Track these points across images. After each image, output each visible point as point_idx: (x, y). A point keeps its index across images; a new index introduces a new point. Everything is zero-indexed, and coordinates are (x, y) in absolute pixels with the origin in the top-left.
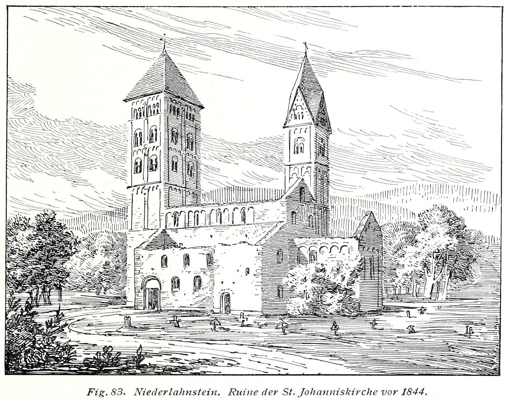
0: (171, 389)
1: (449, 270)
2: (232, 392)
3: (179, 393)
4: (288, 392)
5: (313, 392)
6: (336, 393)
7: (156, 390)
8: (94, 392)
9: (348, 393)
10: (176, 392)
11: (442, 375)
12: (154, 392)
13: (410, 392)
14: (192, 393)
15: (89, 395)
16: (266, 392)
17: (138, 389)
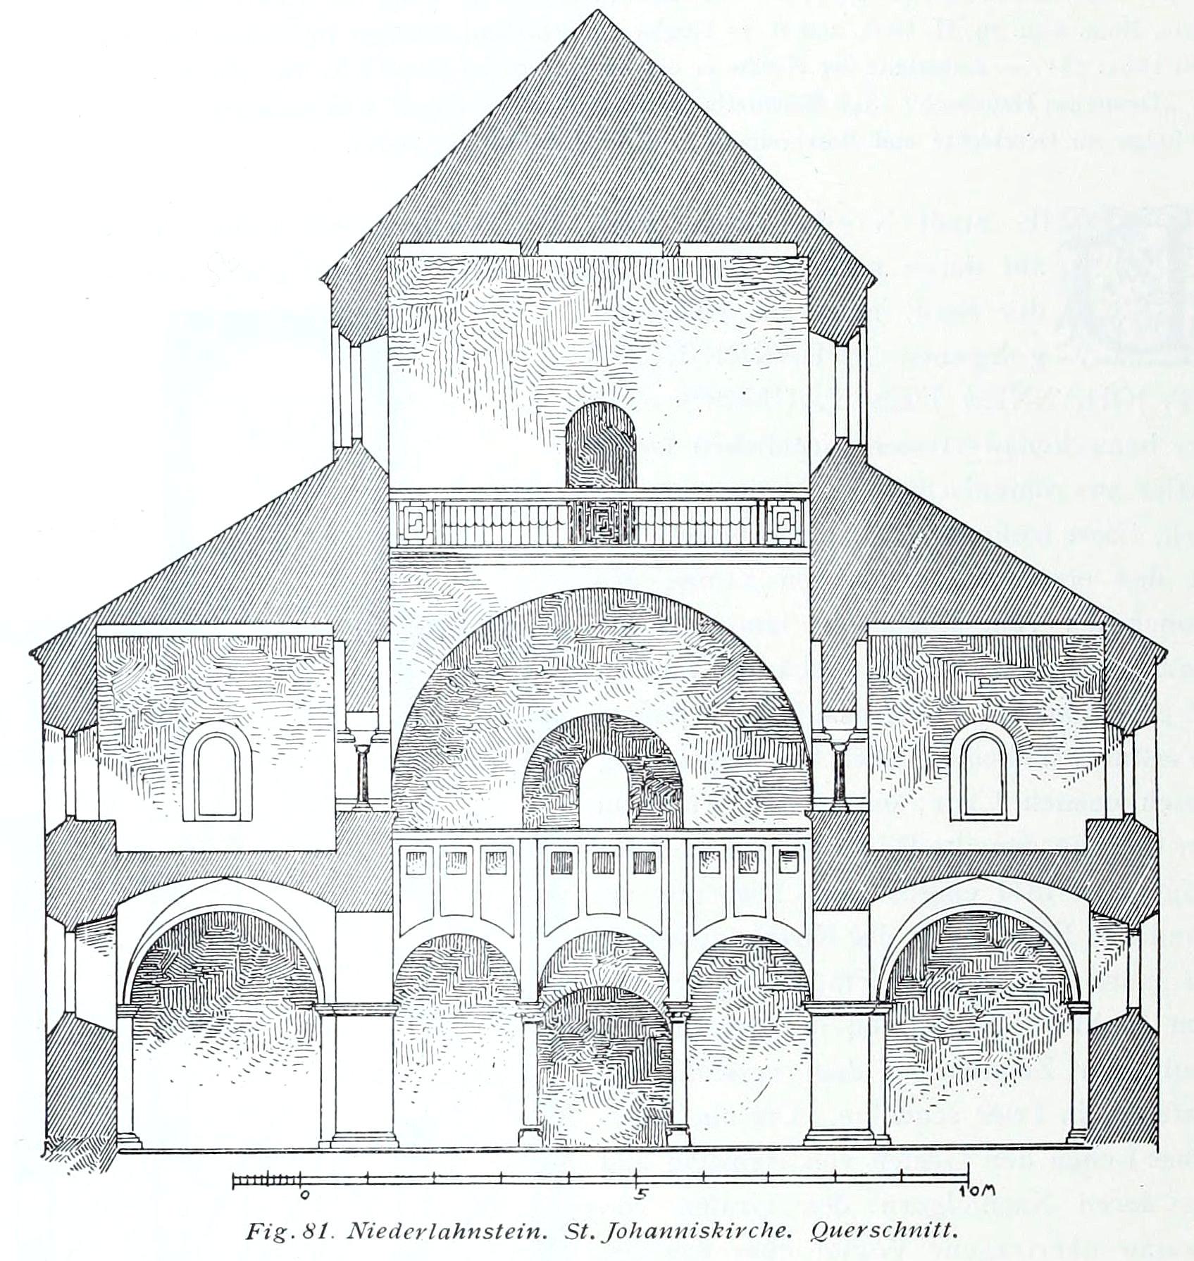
0: (435, 1225)
2: (614, 1231)
3: (451, 1234)
4: (578, 1231)
5: (635, 1231)
6: (689, 1233)
7: (398, 1226)
8: (262, 1233)
9: (718, 1234)
10: (651, 1231)
11: (880, 1175)
12: (395, 1231)
13: (311, 1231)
14: (482, 1233)
15: (250, 1237)
16: (399, 1230)
17: (356, 1224)
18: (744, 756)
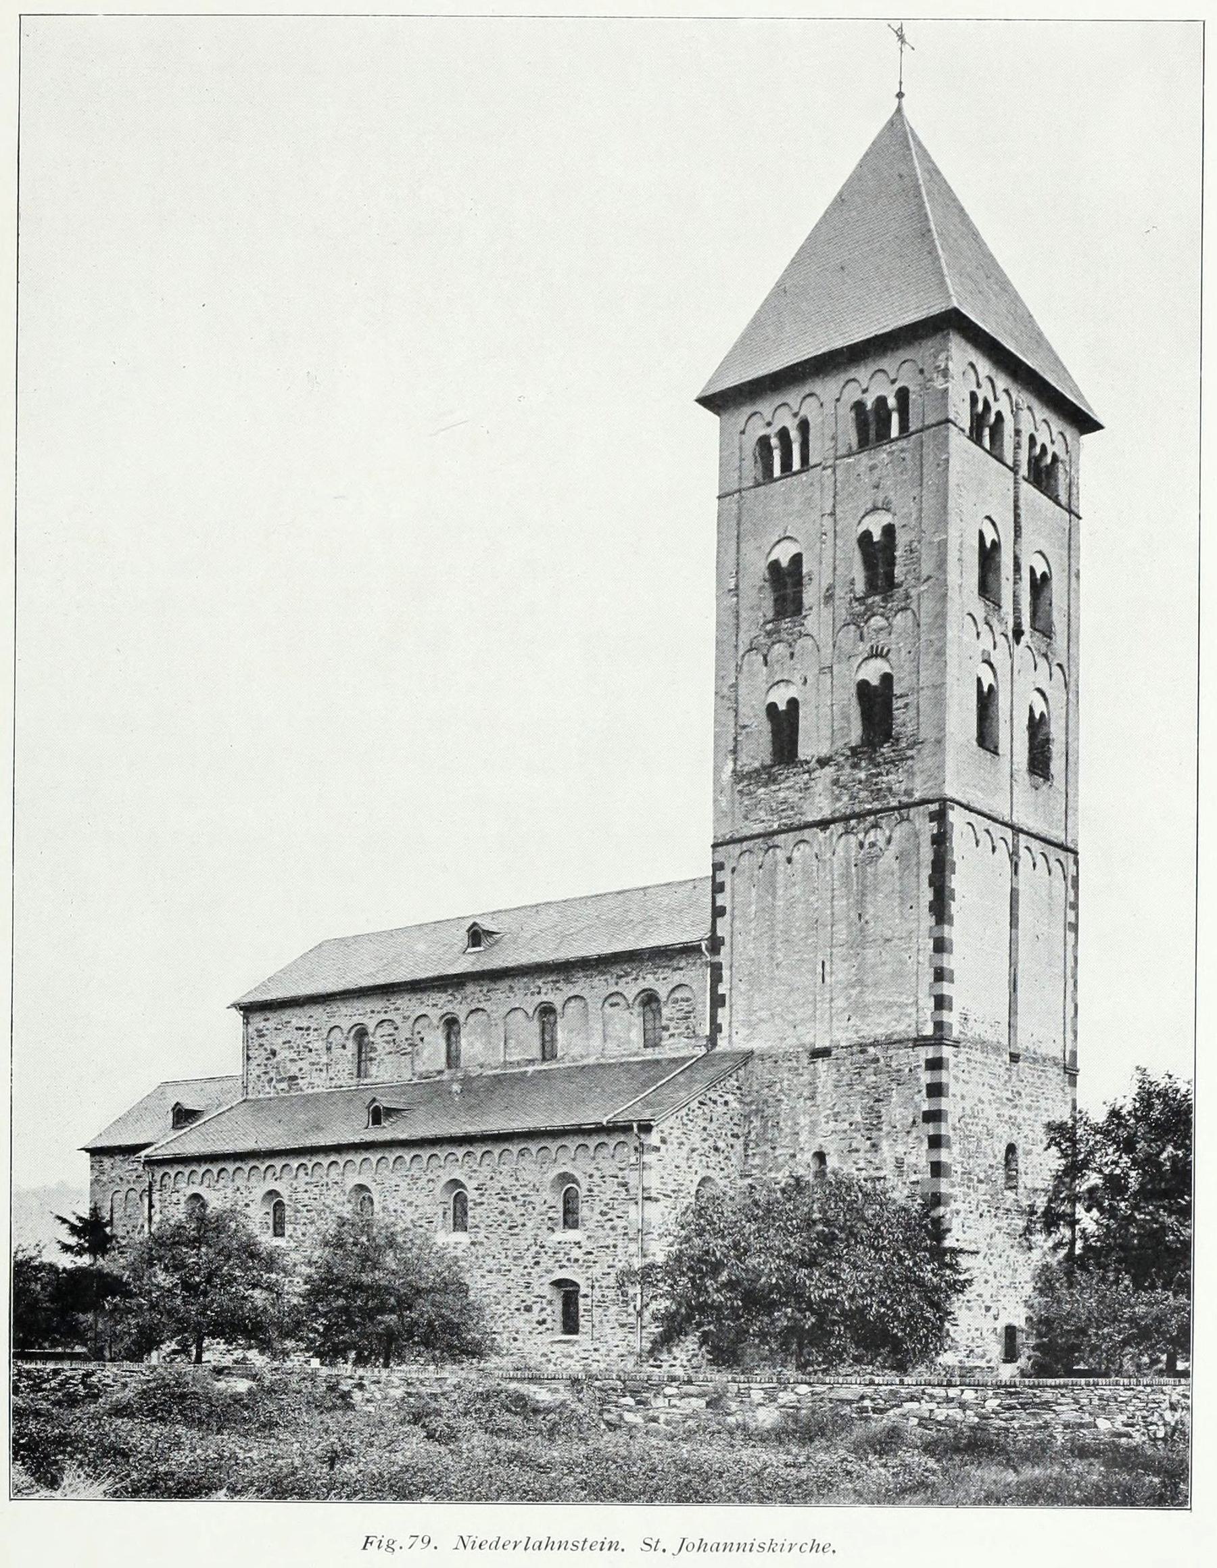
4: (650, 1545)
5: (702, 1546)
8: (376, 1544)
12: (494, 1544)
14: (570, 1546)
15: (364, 1548)
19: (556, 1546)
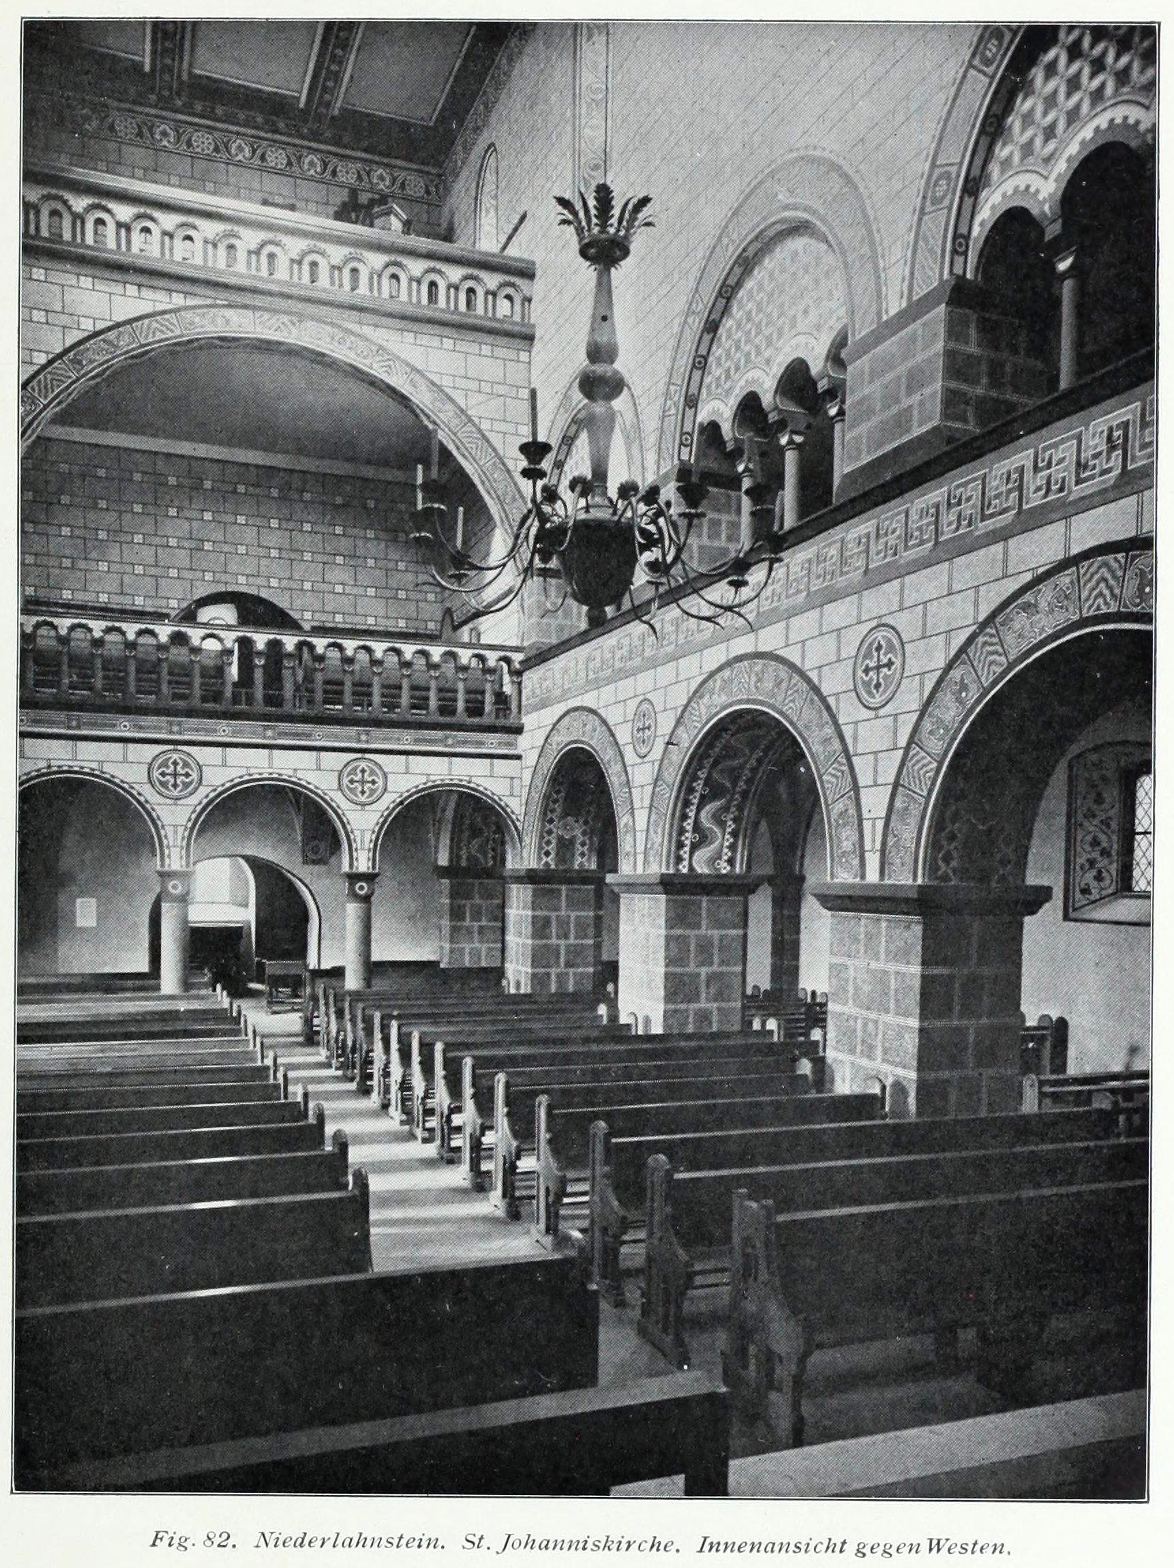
1: (432, 297)
3: (354, 1543)
4: (474, 1542)
5: (530, 1543)
6: (581, 1545)
8: (166, 1541)
12: (300, 1541)
15: (154, 1545)
18: (46, 927)
19: (369, 1543)
